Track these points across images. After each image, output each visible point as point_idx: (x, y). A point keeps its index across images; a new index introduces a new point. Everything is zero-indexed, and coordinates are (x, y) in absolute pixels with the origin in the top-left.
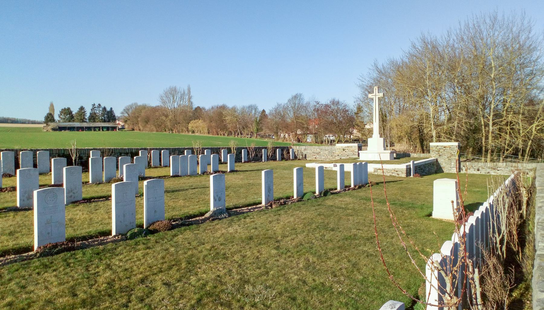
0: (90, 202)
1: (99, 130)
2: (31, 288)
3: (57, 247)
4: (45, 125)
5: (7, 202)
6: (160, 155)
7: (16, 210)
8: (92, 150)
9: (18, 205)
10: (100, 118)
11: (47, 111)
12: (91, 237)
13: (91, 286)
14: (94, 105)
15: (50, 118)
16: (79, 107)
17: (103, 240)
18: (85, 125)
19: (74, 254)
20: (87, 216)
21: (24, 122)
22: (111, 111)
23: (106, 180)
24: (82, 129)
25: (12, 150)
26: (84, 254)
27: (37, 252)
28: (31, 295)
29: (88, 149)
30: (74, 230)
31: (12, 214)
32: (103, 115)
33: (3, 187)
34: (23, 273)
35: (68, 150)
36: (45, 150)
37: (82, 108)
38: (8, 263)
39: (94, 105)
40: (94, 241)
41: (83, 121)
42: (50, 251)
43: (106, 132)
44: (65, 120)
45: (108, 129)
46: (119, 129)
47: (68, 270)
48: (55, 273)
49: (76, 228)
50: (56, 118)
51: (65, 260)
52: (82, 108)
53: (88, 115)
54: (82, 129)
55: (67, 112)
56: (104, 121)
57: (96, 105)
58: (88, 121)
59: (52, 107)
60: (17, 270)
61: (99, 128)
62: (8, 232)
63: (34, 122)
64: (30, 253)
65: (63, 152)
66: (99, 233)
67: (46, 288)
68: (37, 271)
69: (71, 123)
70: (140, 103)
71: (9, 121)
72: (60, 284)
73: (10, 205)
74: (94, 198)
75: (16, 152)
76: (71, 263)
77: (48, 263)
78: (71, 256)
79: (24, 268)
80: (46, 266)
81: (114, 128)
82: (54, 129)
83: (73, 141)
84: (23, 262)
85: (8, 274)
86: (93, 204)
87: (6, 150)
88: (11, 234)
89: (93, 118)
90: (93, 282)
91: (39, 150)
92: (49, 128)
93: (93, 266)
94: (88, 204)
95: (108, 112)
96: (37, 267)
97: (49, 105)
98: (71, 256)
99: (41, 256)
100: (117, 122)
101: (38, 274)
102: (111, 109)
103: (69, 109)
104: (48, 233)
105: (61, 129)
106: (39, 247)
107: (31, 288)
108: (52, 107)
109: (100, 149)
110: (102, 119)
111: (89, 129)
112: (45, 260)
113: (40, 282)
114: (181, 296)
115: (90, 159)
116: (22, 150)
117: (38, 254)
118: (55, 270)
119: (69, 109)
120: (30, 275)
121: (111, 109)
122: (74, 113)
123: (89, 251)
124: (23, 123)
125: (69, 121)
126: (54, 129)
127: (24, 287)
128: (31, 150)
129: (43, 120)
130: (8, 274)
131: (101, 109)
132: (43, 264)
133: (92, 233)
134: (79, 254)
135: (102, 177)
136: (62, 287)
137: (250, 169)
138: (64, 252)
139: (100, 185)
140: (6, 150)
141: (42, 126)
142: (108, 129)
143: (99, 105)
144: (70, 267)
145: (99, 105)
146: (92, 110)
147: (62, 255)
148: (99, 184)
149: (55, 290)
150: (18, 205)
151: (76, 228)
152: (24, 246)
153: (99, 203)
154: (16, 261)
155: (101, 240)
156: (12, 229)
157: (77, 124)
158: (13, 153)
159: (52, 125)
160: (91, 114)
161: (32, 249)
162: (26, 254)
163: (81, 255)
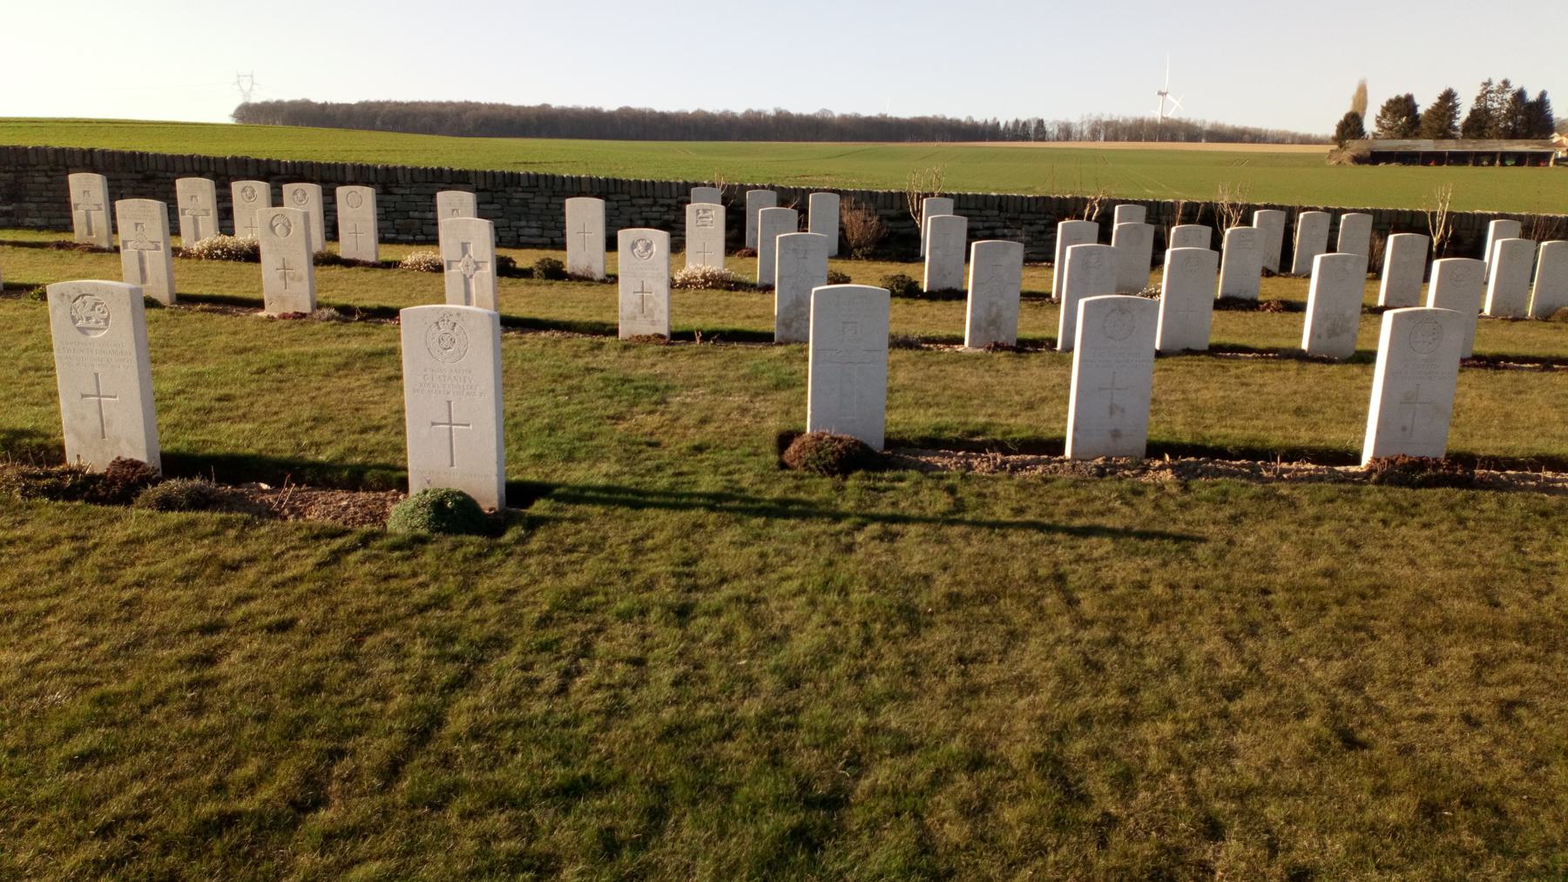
0: (1498, 368)
1: (1492, 163)
2: (1371, 550)
3: (1424, 470)
4: (1335, 147)
5: (1275, 335)
6: (1537, 252)
7: (1301, 357)
8: (1494, 217)
9: (1305, 345)
10: (1502, 125)
11: (1347, 108)
12: (1513, 464)
13: (1539, 595)
14: (1489, 83)
15: (1351, 126)
16: (1441, 92)
17: (1554, 481)
18: (1449, 146)
19: (1473, 498)
20: (1493, 405)
21: (1280, 139)
22: (1542, 103)
23: (1535, 312)
24: (1438, 159)
25: (1281, 208)
26: (1502, 504)
27: (1371, 471)
28: (1377, 568)
29: (1481, 215)
30: (1463, 435)
31: (1293, 366)
32: (1511, 114)
33: (1260, 298)
34: (1346, 510)
35: (1423, 215)
36: (1361, 211)
37: (1448, 96)
38: (1302, 479)
39: (1489, 83)
40: (1525, 478)
41: (1445, 132)
42: (1403, 473)
43: (1513, 172)
44: (1391, 132)
45: (1521, 159)
46: (1558, 161)
47: (1463, 534)
48: (1427, 532)
49: (1468, 430)
50: (1370, 125)
51: (1452, 508)
52: (1448, 96)
53: (1463, 114)
54: (1438, 159)
55: (1402, 107)
56: (1512, 135)
57: (1497, 83)
58: (1460, 134)
59: (1361, 97)
60: (1331, 501)
61: (1504, 157)
62: (1291, 406)
63: (1306, 140)
64: (1352, 469)
65: (1408, 220)
66: (1538, 457)
67: (1412, 562)
68: (1380, 515)
69: (1408, 142)
70: (755, 109)
71: (1182, 135)
72: (1448, 564)
73: (1284, 343)
74: (1507, 358)
75: (1291, 214)
76: (1468, 519)
77: (1405, 504)
78: (1467, 501)
79: (1346, 500)
80: (1400, 509)
81: (1539, 159)
82: (1359, 160)
83: (1440, 193)
84: (1342, 486)
85: (1312, 503)
86: (1507, 374)
87: (1266, 207)
88: (1298, 411)
89: (1480, 122)
90: (1544, 588)
91: (1345, 211)
92: (1347, 154)
93: (1536, 544)
94: (1490, 371)
95: (1531, 105)
96: (1378, 506)
97: (1353, 91)
98: (1467, 501)
99: (1379, 482)
100: (1556, 138)
101: (1385, 522)
102: (1543, 95)
103: (1409, 98)
104: (1404, 429)
105: (1376, 158)
106: (1376, 459)
107: (1371, 550)
108: (1361, 97)
109: (1519, 218)
110: (1507, 128)
111: (1459, 159)
112: (1398, 494)
113: (1393, 542)
114: (550, 548)
115: (1168, 253)
116: (1305, 210)
117: (1374, 477)
118: (1426, 526)
119: (1409, 98)
120: (1365, 521)
121: (1543, 95)
122: (1421, 111)
123: (1516, 502)
124: (1278, 142)
125: (1405, 136)
126: (1359, 160)
127: (1354, 545)
128: (1327, 210)
129: (1332, 131)
130: (1312, 503)
131: (1508, 96)
132: (1392, 502)
133: (1517, 454)
134: (1489, 502)
135: (1526, 302)
136: (1454, 573)
137: (554, 314)
138: (1445, 486)
139: (1518, 325)
140: (1266, 207)
141: (1326, 149)
142: (1521, 159)
143: (1506, 83)
144: (1465, 528)
145: (1506, 83)
146: (1478, 99)
147: (1440, 492)
148: (1515, 320)
149: (1435, 574)
150: (1305, 345)
151: (1468, 430)
152: (1335, 446)
153: (1525, 375)
154: (1321, 479)
155: (1547, 480)
156: (1299, 400)
157: (1426, 145)
158: (1283, 215)
159: (1355, 146)
160: (1473, 112)
161: (1356, 460)
162: (1342, 468)
163: (1494, 506)
